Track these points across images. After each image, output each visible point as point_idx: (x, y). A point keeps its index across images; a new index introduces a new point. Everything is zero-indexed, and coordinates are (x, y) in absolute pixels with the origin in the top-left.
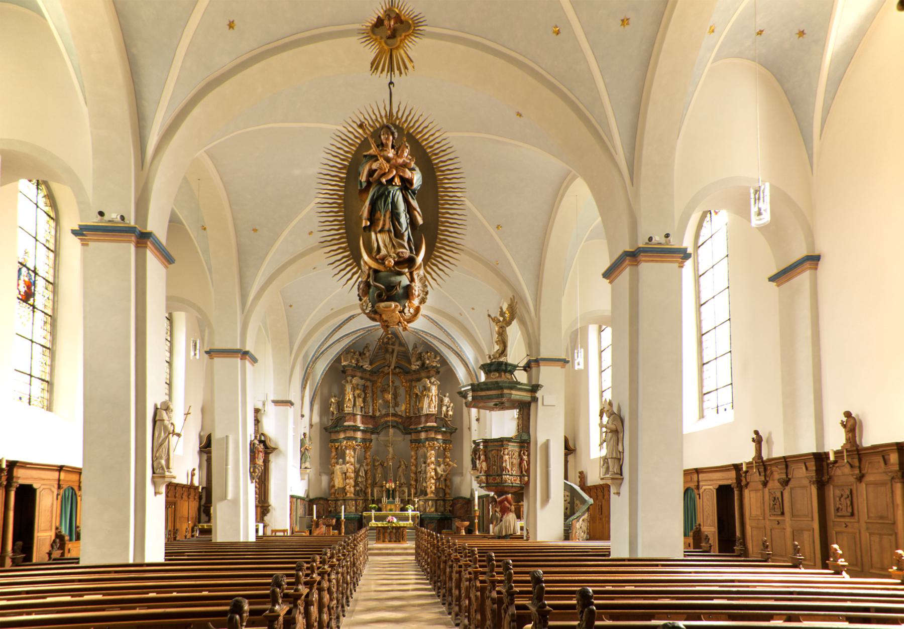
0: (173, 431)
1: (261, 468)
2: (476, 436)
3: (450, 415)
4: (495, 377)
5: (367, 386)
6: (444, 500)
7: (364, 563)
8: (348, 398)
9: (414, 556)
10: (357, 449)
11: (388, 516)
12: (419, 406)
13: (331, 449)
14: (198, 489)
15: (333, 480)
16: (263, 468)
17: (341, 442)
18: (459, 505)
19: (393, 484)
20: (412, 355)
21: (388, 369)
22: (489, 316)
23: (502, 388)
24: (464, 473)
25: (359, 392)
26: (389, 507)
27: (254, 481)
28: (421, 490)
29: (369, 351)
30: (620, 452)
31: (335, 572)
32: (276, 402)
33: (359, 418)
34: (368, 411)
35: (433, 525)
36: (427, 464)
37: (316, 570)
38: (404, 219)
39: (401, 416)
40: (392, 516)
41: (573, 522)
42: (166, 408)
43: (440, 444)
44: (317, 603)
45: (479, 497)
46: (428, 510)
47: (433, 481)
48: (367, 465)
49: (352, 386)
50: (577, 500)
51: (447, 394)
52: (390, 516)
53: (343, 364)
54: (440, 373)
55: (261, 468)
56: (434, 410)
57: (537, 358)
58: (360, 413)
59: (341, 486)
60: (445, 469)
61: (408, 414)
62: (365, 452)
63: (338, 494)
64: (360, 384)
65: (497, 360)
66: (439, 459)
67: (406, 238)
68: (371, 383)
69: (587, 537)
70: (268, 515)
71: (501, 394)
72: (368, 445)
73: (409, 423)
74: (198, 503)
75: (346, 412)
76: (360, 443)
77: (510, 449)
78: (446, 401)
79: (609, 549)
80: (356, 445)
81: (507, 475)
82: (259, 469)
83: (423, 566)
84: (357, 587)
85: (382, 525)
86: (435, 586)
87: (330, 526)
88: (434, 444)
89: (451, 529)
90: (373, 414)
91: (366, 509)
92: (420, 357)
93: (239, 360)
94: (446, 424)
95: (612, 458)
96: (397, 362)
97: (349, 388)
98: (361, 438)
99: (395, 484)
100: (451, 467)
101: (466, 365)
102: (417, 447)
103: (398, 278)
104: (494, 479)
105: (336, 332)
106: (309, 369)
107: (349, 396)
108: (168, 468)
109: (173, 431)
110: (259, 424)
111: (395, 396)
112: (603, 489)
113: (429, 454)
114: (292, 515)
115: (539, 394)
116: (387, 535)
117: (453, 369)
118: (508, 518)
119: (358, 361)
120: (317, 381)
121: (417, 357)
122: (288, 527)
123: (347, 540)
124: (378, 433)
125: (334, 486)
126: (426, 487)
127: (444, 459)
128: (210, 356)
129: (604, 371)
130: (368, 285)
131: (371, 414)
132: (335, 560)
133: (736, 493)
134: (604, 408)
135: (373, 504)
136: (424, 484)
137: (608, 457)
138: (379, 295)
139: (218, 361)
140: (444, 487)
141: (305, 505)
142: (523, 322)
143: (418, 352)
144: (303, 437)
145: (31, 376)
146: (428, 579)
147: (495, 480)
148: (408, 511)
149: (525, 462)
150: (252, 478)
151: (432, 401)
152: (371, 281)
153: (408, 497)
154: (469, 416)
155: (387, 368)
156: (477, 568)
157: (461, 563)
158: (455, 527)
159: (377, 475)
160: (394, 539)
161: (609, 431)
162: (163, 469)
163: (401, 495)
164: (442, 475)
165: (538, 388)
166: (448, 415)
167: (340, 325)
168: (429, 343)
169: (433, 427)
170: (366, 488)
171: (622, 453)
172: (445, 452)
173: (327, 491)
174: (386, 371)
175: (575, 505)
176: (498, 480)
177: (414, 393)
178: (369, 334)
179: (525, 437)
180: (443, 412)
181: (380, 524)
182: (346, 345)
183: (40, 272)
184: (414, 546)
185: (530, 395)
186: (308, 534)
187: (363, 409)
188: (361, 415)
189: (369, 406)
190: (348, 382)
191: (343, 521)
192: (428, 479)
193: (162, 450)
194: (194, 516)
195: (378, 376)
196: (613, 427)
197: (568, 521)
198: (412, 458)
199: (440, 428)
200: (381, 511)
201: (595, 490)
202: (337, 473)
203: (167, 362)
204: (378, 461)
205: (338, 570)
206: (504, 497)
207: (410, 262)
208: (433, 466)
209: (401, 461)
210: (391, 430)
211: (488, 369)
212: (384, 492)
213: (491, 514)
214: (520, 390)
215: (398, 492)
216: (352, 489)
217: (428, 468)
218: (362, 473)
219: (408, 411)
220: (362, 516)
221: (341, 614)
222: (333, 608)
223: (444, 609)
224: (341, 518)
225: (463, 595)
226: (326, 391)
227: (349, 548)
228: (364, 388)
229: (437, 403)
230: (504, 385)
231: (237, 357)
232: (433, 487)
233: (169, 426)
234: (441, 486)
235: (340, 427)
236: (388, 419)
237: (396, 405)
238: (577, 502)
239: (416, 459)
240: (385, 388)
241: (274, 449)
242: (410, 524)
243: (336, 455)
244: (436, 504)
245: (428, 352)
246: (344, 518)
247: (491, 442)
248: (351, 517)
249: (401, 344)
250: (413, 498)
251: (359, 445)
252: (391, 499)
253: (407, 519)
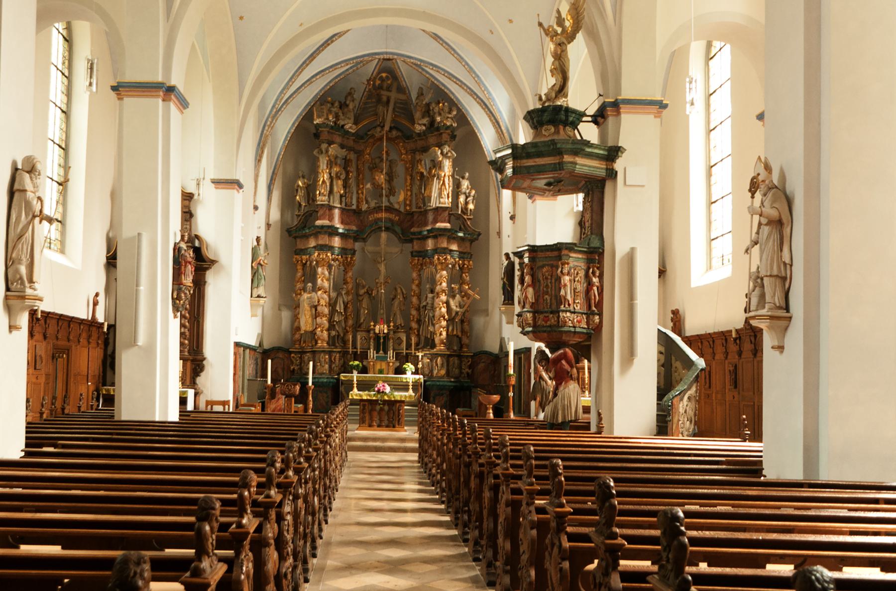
0: (41, 211)
1: (189, 291)
2: (508, 247)
3: (471, 210)
4: (548, 132)
5: (350, 160)
6: (460, 357)
7: (340, 466)
8: (322, 179)
9: (417, 454)
10: (333, 265)
11: (377, 382)
12: (425, 195)
13: (296, 265)
14: (103, 328)
15: (298, 318)
16: (192, 292)
17: (310, 255)
18: (481, 366)
19: (386, 326)
20: (415, 107)
21: (380, 132)
22: (540, 25)
23: (560, 153)
24: (490, 311)
25: (338, 170)
26: (378, 367)
27: (179, 314)
28: (426, 338)
29: (353, 101)
30: (785, 264)
31: (291, 498)
32: (217, 183)
33: (337, 212)
34: (351, 203)
35: (444, 399)
36: (435, 294)
37: (248, 507)
39: (397, 212)
40: (384, 382)
41: (675, 400)
42: (29, 169)
43: (455, 259)
44: (251, 581)
45: (516, 352)
46: (435, 372)
47: (444, 323)
48: (347, 293)
49: (327, 158)
50: (676, 360)
51: (467, 174)
52: (380, 382)
53: (315, 122)
54: (457, 139)
55: (189, 291)
56: (447, 202)
57: (617, 100)
58: (339, 206)
59: (309, 329)
60: (462, 303)
61: (408, 208)
62: (345, 272)
63: (305, 342)
64: (339, 155)
65: (551, 104)
66: (453, 286)
68: (356, 155)
69: (694, 429)
70: (203, 374)
71: (559, 163)
72: (349, 259)
73: (410, 223)
74: (102, 350)
75: (318, 203)
76: (338, 255)
77: (571, 265)
78: (465, 187)
79: (761, 457)
80: (333, 260)
81: (566, 311)
82: (185, 294)
83: (434, 476)
84: (329, 513)
85: (369, 398)
86: (457, 519)
87: (291, 397)
88: (445, 259)
89: (470, 407)
90: (358, 206)
91: (345, 368)
92: (427, 111)
93: (160, 101)
94: (464, 226)
95: (771, 276)
96: (393, 121)
97: (323, 163)
98: (339, 248)
99: (389, 326)
100: (471, 299)
101: (496, 123)
102: (422, 265)
105: (307, 65)
106: (266, 128)
107: (323, 177)
108: (31, 281)
109: (41, 211)
110: (193, 220)
111: (390, 177)
112: (713, 342)
113: (438, 276)
114: (237, 376)
115: (619, 165)
116: (375, 414)
117: (476, 131)
118: (567, 390)
119: (337, 117)
120: (278, 151)
121: (423, 110)
122: (230, 397)
123: (314, 427)
124: (364, 240)
125: (299, 329)
126: (433, 333)
127: (461, 285)
128: (118, 94)
129: (714, 129)
131: (354, 207)
132: (291, 473)
134: (759, 174)
135: (355, 360)
136: (431, 328)
137: (762, 274)
139: (132, 103)
140: (460, 334)
141: (256, 359)
142: (593, 37)
143: (424, 103)
144: (255, 243)
146: (443, 502)
147: (548, 320)
148: (405, 374)
149: (595, 288)
150: (176, 308)
151: (445, 186)
153: (407, 349)
154: (499, 211)
155: (379, 129)
156: (562, 506)
157: (498, 471)
158: (477, 403)
159: (362, 311)
160: (386, 422)
161: (764, 221)
162: (23, 283)
163: (396, 347)
164: (457, 313)
165: (617, 154)
166: (466, 209)
167: (312, 55)
168: (441, 86)
169: (445, 230)
170: (346, 332)
171: (788, 267)
172: (462, 273)
173: (289, 337)
174: (377, 135)
175: (673, 369)
176: (553, 321)
177: (418, 173)
178: (354, 71)
179: (595, 243)
180: (460, 205)
181: (365, 395)
182: (321, 91)
184: (417, 435)
185: (605, 167)
186: (258, 409)
187: (343, 199)
188: (340, 208)
189: (353, 193)
190: (322, 153)
191: (310, 387)
192: (436, 319)
193: (22, 248)
194: (97, 373)
195: (365, 142)
196: (774, 213)
197: (665, 399)
198: (413, 282)
199: (457, 232)
200: (367, 373)
201: (699, 344)
202: (304, 306)
203: (63, 112)
204: (364, 287)
205: (298, 490)
206: (561, 351)
208: (444, 297)
209: (397, 287)
210: (384, 235)
211: (536, 118)
212: (372, 340)
213: (533, 382)
214: (590, 156)
215: (391, 341)
216: (325, 334)
217: (437, 300)
218: (340, 307)
219: (408, 202)
220: (338, 379)
221: (302, 578)
222: (286, 575)
223: (476, 571)
224: (307, 383)
225: (525, 558)
226: (290, 168)
227: (318, 442)
228: (345, 162)
229: (451, 188)
230: (564, 146)
231: (158, 96)
232: (444, 333)
233: (35, 202)
234: (455, 333)
235: (309, 228)
236: (379, 215)
237: (392, 192)
238: (677, 364)
239: (419, 285)
240: (375, 164)
241: (213, 262)
242: (410, 396)
243: (303, 275)
244: (448, 362)
245: (439, 103)
246: (313, 383)
247: (542, 251)
248: (322, 382)
249: (402, 90)
250: (413, 352)
251: (337, 259)
252: (381, 352)
253: (405, 387)
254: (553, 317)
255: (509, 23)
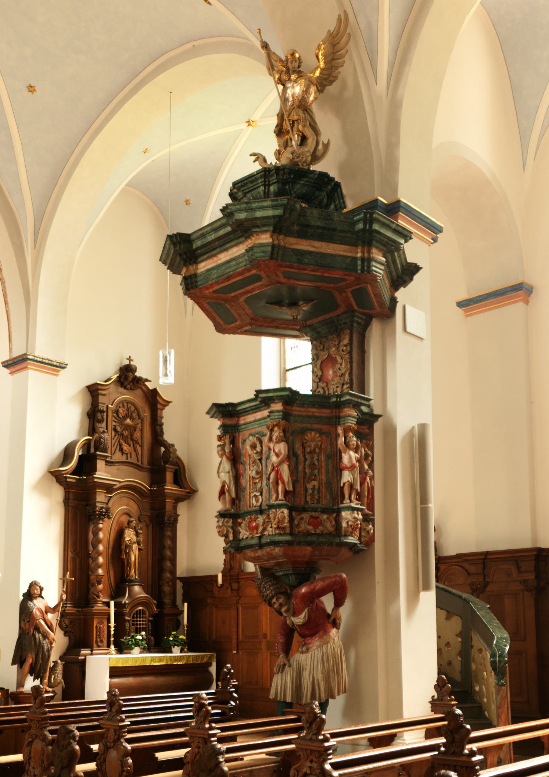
104: (315, 522)
176: (329, 526)
254: (328, 518)
255: (27, 90)
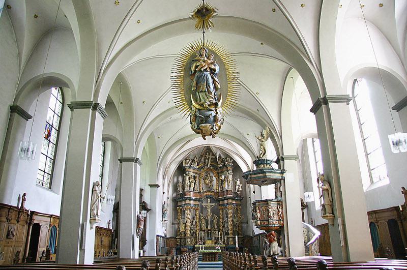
22: (256, 136)
33: (192, 193)
38: (212, 87)
56: (231, 188)
67: (213, 94)
103: (210, 112)
130: (196, 116)
132: (178, 264)
133: (399, 224)
138: (202, 121)
145: (47, 156)
150: (137, 235)
152: (198, 114)
176: (267, 223)
183: (54, 126)
207: (216, 105)
220: (194, 247)
